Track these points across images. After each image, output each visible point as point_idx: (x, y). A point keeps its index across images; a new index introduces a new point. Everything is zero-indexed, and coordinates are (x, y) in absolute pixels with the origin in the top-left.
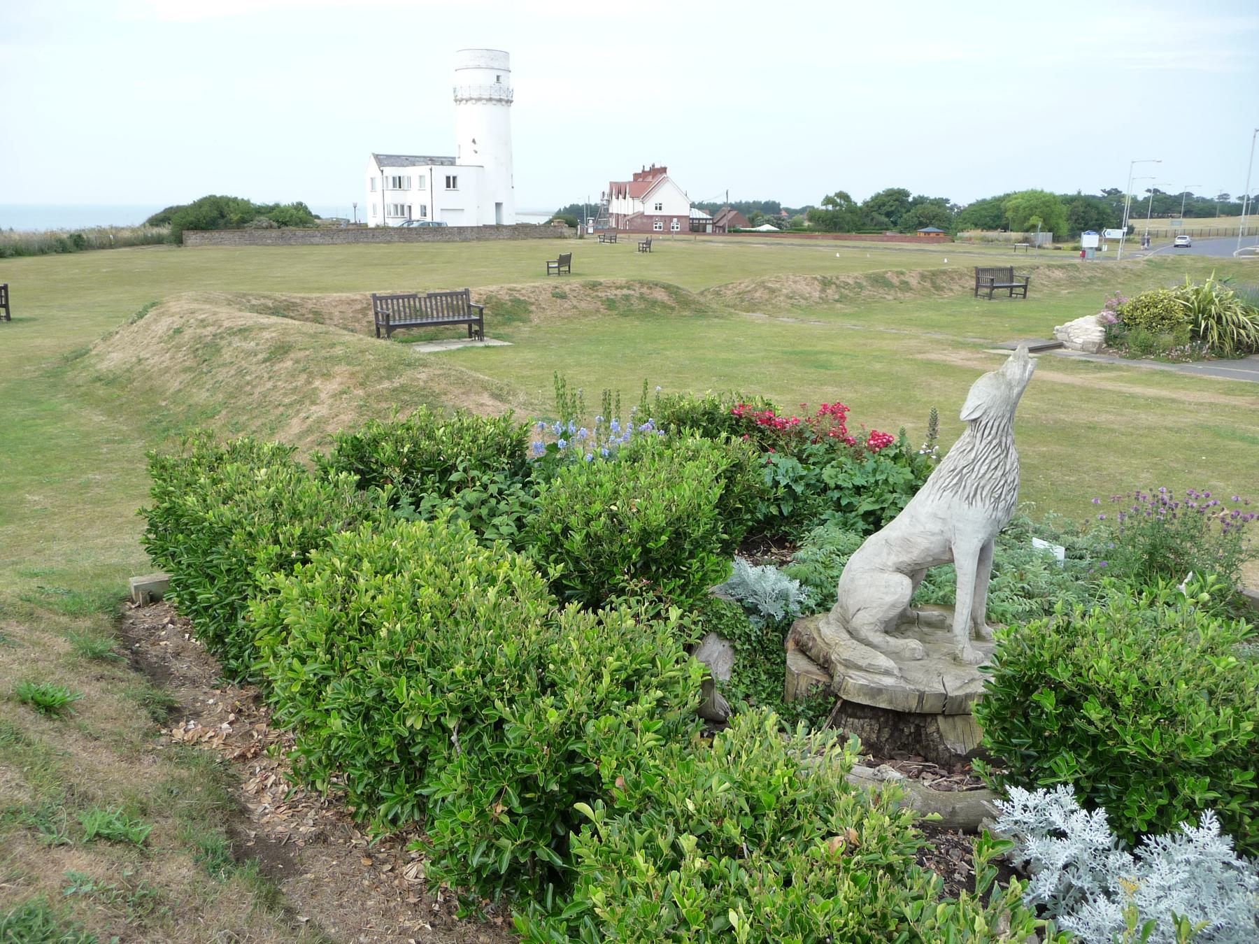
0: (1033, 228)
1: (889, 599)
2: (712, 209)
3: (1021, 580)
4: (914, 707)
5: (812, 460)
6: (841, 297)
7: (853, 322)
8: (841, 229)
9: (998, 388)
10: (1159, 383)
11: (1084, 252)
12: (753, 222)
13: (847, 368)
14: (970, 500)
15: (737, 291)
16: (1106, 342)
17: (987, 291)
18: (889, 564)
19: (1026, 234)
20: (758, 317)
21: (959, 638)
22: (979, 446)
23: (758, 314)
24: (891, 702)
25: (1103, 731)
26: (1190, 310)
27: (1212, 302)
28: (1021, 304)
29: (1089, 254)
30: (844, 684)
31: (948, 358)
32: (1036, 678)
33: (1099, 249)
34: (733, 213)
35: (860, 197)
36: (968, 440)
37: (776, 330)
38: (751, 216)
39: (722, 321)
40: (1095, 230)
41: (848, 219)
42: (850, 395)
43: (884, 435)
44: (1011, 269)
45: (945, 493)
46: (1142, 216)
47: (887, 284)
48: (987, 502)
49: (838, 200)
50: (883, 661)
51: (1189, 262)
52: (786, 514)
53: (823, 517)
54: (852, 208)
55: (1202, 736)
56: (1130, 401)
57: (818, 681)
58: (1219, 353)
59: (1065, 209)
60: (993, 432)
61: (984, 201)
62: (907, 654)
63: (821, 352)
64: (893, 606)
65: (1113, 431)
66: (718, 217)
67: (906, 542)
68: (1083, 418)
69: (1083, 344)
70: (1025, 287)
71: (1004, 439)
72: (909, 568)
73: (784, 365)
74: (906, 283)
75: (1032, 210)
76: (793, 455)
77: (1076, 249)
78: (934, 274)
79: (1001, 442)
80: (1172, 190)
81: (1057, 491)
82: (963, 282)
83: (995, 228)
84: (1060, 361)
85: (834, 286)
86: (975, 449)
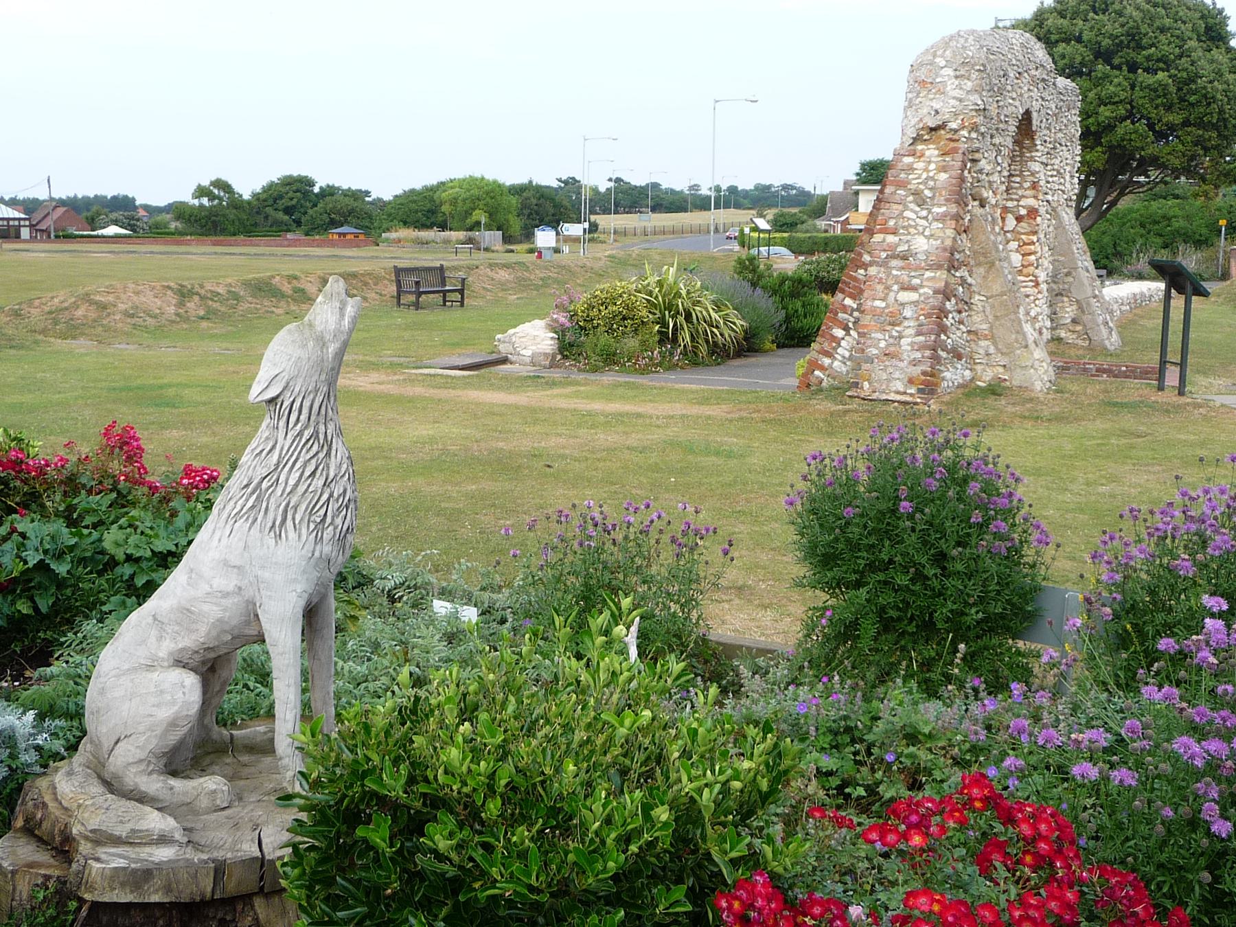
0: (476, 226)
1: (165, 714)
2: (30, 206)
3: (407, 661)
4: (209, 889)
5: (88, 520)
6: (208, 312)
7: (224, 345)
8: (223, 231)
10: (622, 397)
11: (540, 253)
12: (92, 223)
13: (205, 404)
14: (277, 529)
15: (47, 309)
16: (561, 353)
17: (412, 298)
18: (161, 655)
19: (470, 233)
20: (81, 345)
21: (285, 761)
22: (284, 442)
23: (82, 341)
24: (168, 889)
25: (461, 868)
26: (655, 306)
27: (678, 295)
28: (457, 313)
29: (547, 256)
30: (87, 872)
31: (354, 383)
32: (362, 799)
33: (557, 251)
34: (61, 210)
35: (247, 186)
36: (267, 434)
37: (106, 360)
38: (89, 214)
39: (22, 352)
40: (548, 225)
41: (232, 217)
42: (205, 439)
43: (204, 469)
44: (441, 268)
46: (606, 211)
47: (277, 294)
48: (304, 531)
49: (216, 191)
50: (155, 821)
51: (657, 257)
52: (44, 609)
54: (237, 203)
55: (603, 842)
56: (588, 420)
57: (47, 878)
58: (693, 360)
59: (514, 201)
60: (304, 417)
61: (413, 191)
62: (204, 803)
63: (170, 386)
64: (173, 724)
65: (564, 457)
66: (37, 216)
67: (186, 614)
68: (526, 445)
69: (533, 356)
70: (461, 292)
71: (322, 428)
72: (197, 658)
74: (303, 291)
75: (474, 202)
77: (531, 251)
79: (316, 432)
80: (638, 179)
81: (488, 540)
82: (379, 287)
83: (430, 227)
84: (502, 378)
85: (196, 298)
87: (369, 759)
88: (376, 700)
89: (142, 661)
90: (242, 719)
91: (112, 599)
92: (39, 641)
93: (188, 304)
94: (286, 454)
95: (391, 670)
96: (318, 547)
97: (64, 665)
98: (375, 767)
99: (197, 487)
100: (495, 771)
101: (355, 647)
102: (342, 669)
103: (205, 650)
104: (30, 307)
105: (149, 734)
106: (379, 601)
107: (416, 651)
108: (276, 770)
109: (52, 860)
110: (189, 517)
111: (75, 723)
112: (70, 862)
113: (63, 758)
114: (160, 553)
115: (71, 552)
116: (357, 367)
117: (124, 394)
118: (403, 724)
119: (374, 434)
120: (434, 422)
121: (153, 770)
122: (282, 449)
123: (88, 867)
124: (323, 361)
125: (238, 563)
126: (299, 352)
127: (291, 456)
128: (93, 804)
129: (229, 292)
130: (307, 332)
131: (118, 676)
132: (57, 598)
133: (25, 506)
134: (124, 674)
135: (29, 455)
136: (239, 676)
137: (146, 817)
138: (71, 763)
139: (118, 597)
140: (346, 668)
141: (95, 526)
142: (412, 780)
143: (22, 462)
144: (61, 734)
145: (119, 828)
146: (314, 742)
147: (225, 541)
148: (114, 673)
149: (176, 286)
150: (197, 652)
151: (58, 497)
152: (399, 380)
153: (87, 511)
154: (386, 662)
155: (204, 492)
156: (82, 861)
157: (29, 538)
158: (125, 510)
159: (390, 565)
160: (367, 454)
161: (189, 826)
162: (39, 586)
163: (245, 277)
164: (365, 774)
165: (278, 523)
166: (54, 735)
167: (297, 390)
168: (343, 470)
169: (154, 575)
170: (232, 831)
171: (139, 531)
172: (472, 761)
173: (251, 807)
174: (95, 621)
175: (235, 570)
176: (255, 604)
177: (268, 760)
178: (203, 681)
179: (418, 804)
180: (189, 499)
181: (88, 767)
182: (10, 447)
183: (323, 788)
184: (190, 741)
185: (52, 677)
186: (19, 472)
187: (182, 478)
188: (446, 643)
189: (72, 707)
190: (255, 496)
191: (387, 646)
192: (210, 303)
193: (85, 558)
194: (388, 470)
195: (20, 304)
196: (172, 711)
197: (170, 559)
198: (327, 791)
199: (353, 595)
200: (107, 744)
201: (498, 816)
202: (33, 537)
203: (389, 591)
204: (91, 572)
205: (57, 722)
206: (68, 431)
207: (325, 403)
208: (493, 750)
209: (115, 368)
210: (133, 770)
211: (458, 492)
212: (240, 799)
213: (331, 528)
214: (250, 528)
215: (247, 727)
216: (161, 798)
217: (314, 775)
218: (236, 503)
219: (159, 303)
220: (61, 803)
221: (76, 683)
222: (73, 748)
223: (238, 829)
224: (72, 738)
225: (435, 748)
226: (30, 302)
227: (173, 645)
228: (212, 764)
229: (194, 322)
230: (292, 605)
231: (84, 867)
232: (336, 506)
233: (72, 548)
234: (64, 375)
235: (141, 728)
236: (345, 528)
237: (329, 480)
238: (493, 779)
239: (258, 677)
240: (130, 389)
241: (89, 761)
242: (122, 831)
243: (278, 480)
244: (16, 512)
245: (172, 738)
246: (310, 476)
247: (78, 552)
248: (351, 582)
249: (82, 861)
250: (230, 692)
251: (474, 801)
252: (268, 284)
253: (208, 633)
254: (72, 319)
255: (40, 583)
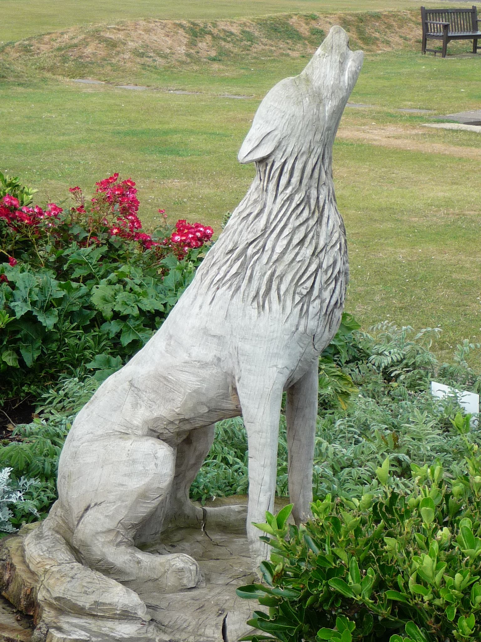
5: (78, 273)
6: (220, 54)
7: (235, 90)
9: (299, 103)
13: (209, 153)
15: (56, 45)
17: (439, 43)
18: (136, 423)
23: (90, 80)
31: (368, 136)
32: (326, 600)
36: (255, 196)
37: (112, 101)
42: (207, 191)
43: (197, 226)
45: (220, 292)
48: (289, 303)
52: (29, 362)
53: (90, 366)
62: (171, 581)
63: (175, 131)
64: (143, 496)
71: (314, 193)
72: (172, 428)
73: (112, 151)
76: (47, 265)
78: (362, 19)
79: (307, 197)
85: (208, 38)
86: (267, 211)
87: (336, 557)
88: (360, 487)
89: (117, 428)
90: (219, 496)
91: (97, 357)
92: (22, 394)
93: (200, 45)
94: (274, 220)
95: (378, 456)
96: (303, 322)
97: (44, 422)
98: (342, 567)
99: (189, 245)
100: (472, 585)
101: (342, 427)
102: (327, 449)
103: (182, 421)
104: (39, 43)
105: (119, 504)
106: (373, 378)
107: (407, 438)
108: (245, 552)
109: (16, 625)
110: (179, 277)
111: (50, 485)
112: (33, 627)
113: (35, 520)
114: (149, 312)
115: (59, 305)
116: (373, 118)
117: (128, 138)
118: (377, 522)
119: (385, 194)
120: (453, 183)
121: (121, 542)
122: (270, 213)
123: (49, 636)
124: (318, 119)
125: (218, 332)
126: (293, 109)
127: (280, 221)
128: (59, 572)
129: (244, 32)
130: (303, 87)
131: (91, 441)
132: (42, 351)
133: (17, 254)
134: (97, 440)
135: (22, 202)
136: (219, 449)
137: (111, 590)
138: (41, 525)
139: (103, 355)
140: (331, 450)
141: (85, 279)
142: (380, 585)
143: (16, 208)
144: (35, 494)
145: (83, 599)
146: (280, 533)
147: (206, 308)
148: (87, 437)
149: (188, 25)
150: (172, 423)
151: (49, 247)
152: (417, 135)
153: (80, 264)
154: (374, 447)
155: (196, 251)
156: (44, 629)
157: (18, 288)
158: (116, 264)
159: (389, 340)
160: (377, 216)
161: (154, 603)
162: (26, 339)
163: (260, 16)
164: (330, 574)
165: (262, 292)
166: (28, 494)
167: (289, 150)
168: (334, 239)
169: (140, 335)
170: (196, 614)
171: (128, 288)
172: (447, 571)
173: (218, 591)
174: (76, 379)
175: (215, 340)
176: (234, 378)
177: (240, 541)
178: (178, 452)
179: (385, 612)
180: (180, 257)
181: (57, 532)
182: (4, 193)
183: (287, 582)
184: (161, 514)
185: (31, 434)
186: (13, 219)
187: (174, 235)
188: (441, 432)
189: (48, 467)
190: (239, 263)
191: (376, 429)
192: (223, 43)
193: (72, 312)
194: (398, 234)
195: (29, 39)
196: (143, 483)
197: (157, 319)
198: (290, 587)
199: (347, 370)
200: (77, 510)
201: (471, 635)
202: (22, 288)
203: (386, 368)
204: (77, 328)
205: (32, 481)
206: (70, 176)
207: (318, 166)
208: (471, 561)
209: (121, 110)
210: (101, 539)
211: (472, 262)
212: (208, 580)
213: (318, 301)
214: (232, 296)
215: (222, 504)
216: (128, 571)
217: (278, 568)
218: (219, 269)
219: (170, 42)
220: (28, 567)
221: (54, 443)
222: (45, 509)
223: (203, 612)
224: (45, 499)
225: (408, 553)
226: (40, 37)
227: (147, 414)
228: (182, 540)
229: (205, 63)
230: (272, 382)
231: (46, 635)
232: (325, 278)
233: (60, 301)
234: (70, 116)
235: (111, 497)
236: (333, 302)
237: (319, 250)
238: (469, 594)
239: (238, 451)
240: (134, 133)
241: (59, 526)
242: (85, 602)
243: (264, 247)
244: (6, 260)
245: (143, 510)
246: (298, 244)
247: (65, 306)
248: (344, 357)
249: (44, 629)
250: (207, 465)
251: (446, 616)
252: (285, 24)
253: (185, 404)
254: (81, 57)
255: (26, 336)
